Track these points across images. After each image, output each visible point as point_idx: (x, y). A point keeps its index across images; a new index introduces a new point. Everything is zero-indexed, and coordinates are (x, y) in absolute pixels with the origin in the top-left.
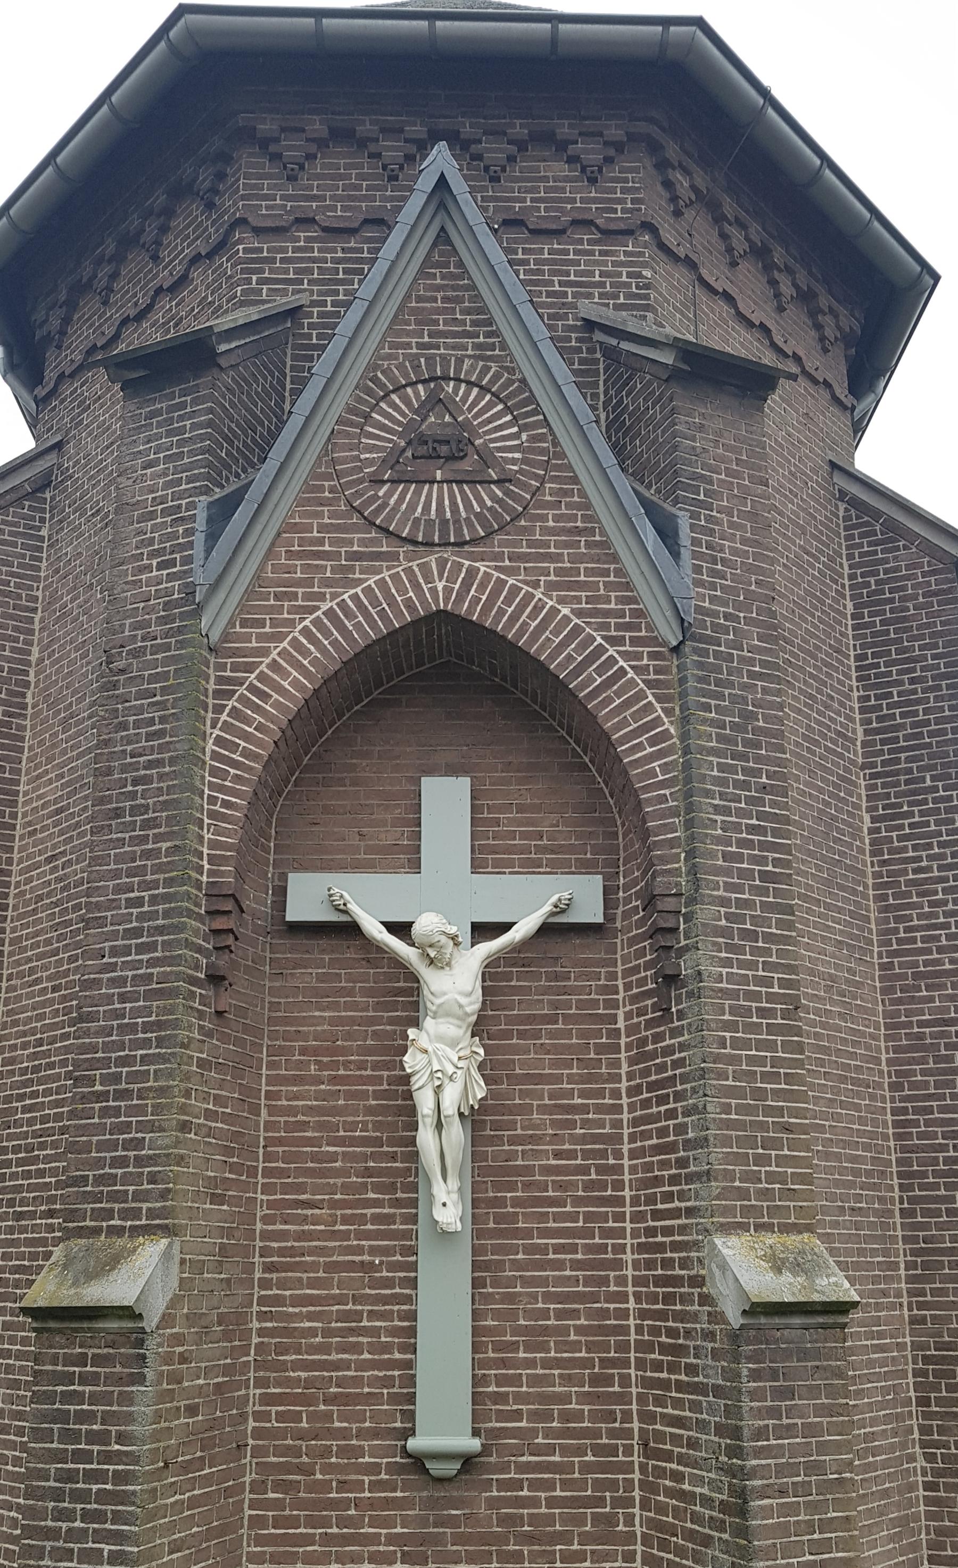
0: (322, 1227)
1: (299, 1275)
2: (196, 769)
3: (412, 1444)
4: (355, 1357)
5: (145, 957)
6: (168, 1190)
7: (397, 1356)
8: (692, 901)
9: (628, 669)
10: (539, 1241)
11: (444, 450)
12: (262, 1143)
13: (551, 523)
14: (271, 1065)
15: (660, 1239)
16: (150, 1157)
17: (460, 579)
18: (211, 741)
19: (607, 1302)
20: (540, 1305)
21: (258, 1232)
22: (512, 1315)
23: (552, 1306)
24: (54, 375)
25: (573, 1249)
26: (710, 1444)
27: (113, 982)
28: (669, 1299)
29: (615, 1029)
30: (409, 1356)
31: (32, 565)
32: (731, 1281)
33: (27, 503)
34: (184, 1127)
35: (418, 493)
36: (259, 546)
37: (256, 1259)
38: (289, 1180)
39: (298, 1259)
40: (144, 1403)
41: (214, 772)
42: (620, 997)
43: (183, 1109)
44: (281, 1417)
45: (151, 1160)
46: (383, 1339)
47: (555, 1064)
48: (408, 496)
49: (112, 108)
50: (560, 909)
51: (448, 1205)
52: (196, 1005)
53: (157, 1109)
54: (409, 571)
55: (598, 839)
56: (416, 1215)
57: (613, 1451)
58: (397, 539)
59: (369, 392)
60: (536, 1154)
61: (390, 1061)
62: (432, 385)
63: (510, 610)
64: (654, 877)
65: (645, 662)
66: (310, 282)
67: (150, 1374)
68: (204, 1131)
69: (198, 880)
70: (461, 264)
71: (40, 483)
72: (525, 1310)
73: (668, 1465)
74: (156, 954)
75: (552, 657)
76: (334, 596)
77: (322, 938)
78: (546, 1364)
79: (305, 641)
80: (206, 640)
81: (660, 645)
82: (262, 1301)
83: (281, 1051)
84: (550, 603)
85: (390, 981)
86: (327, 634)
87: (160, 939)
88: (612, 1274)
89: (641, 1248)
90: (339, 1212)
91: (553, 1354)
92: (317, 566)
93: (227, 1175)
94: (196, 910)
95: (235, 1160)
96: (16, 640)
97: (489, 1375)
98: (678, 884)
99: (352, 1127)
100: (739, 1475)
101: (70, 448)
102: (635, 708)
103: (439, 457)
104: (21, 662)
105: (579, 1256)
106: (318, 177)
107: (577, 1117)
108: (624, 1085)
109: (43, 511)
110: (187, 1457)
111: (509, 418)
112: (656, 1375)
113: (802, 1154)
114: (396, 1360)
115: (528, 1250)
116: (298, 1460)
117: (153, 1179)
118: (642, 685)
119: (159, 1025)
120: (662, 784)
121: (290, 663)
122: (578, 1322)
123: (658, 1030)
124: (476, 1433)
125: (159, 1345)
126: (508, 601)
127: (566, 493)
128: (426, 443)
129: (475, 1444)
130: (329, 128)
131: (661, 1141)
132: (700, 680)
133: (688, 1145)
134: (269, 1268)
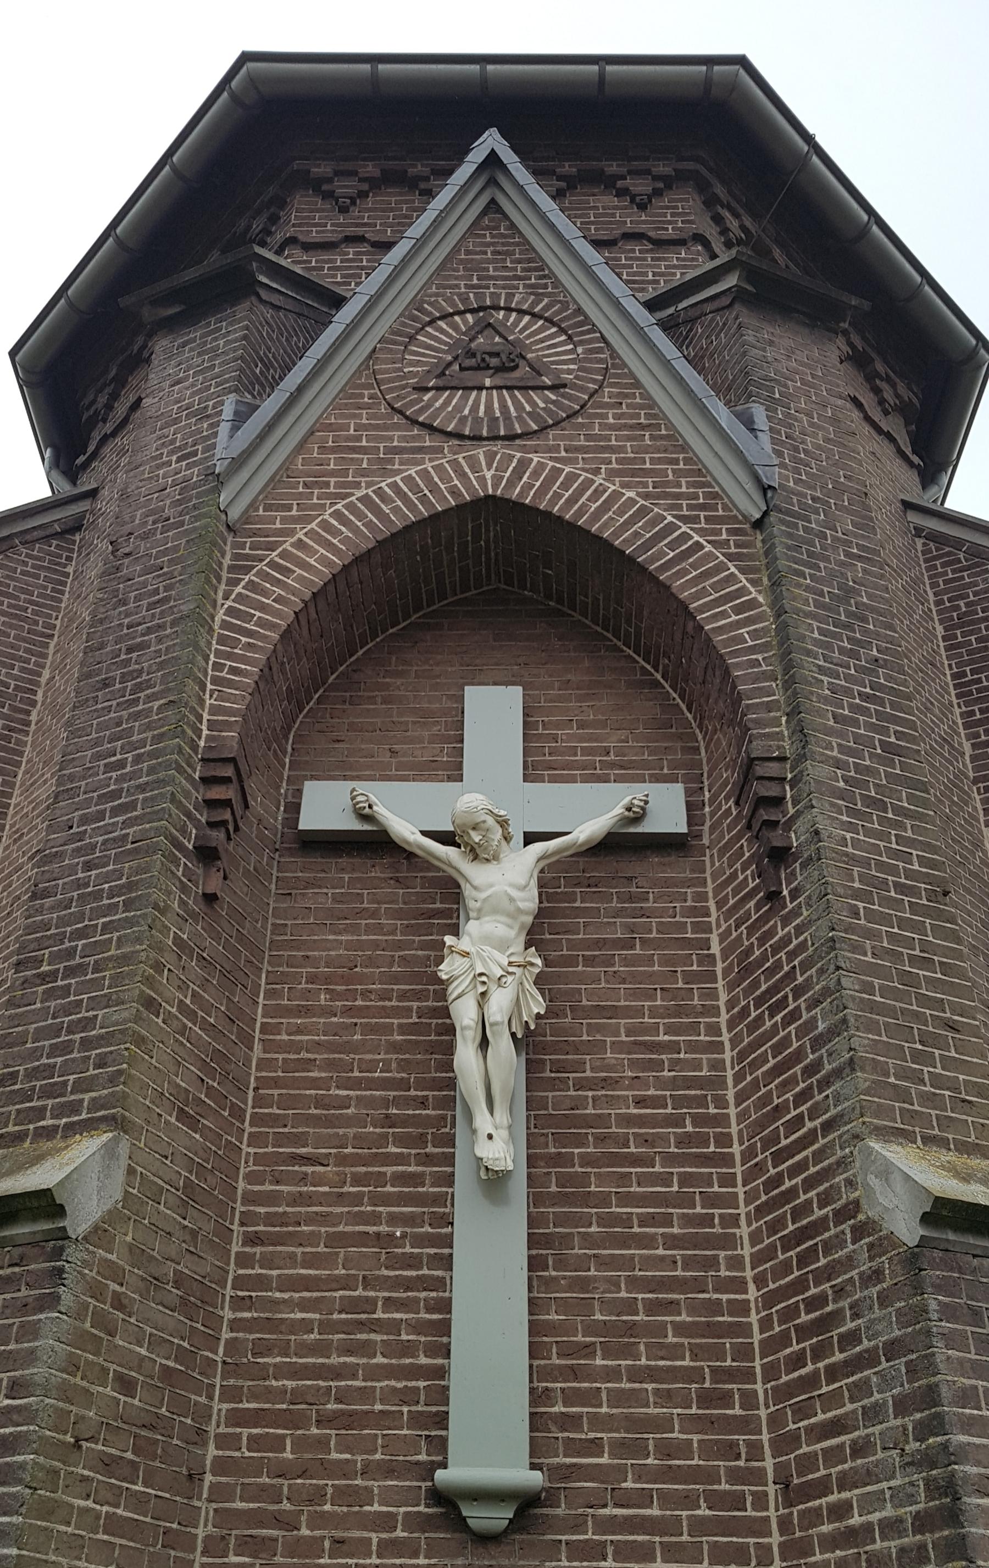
0: (326, 1189)
1: (292, 1249)
4: (364, 1360)
5: (120, 819)
6: (120, 1072)
7: (423, 1360)
8: (802, 757)
9: (705, 543)
10: (618, 1210)
11: (494, 362)
13: (611, 421)
14: (270, 994)
15: (788, 1184)
16: (101, 1037)
17: (511, 469)
18: (222, 612)
19: (716, 1290)
20: (623, 1294)
21: (240, 1192)
22: (585, 1306)
23: (640, 1296)
25: (667, 1221)
29: (709, 956)
30: (440, 1361)
32: (899, 1186)
33: (55, 542)
34: (150, 1004)
35: (465, 399)
38: (286, 1130)
39: (291, 1229)
40: (52, 1338)
41: (222, 640)
44: (254, 1443)
46: (404, 1337)
49: (173, 168)
50: (636, 815)
51: (494, 1139)
52: (180, 874)
54: (455, 464)
56: (453, 1174)
57: (738, 1502)
60: (611, 1101)
62: (481, 314)
63: (567, 495)
64: (750, 742)
65: (724, 536)
69: (193, 740)
70: (513, 226)
71: (71, 524)
75: (616, 534)
77: (341, 857)
78: (636, 1375)
79: (335, 523)
80: (223, 516)
81: (740, 523)
82: (239, 1282)
83: (283, 978)
85: (424, 902)
86: (361, 516)
87: (141, 797)
88: (722, 1254)
90: (347, 1170)
91: (643, 1361)
92: (352, 459)
93: (203, 1096)
94: (189, 770)
95: (215, 1085)
96: (27, 661)
97: (552, 1390)
101: (105, 492)
102: (715, 579)
103: (488, 367)
104: (31, 682)
105: (676, 1230)
106: (369, 210)
107: (664, 1057)
109: (72, 551)
110: (113, 1451)
113: (975, 1060)
114: (421, 1366)
115: (603, 1220)
116: (276, 1507)
118: (722, 558)
120: (752, 650)
121: (316, 544)
122: (678, 1319)
124: (533, 1467)
125: (85, 1263)
126: (565, 486)
127: (626, 396)
128: (474, 355)
129: (536, 1479)
131: (780, 1058)
132: (789, 548)
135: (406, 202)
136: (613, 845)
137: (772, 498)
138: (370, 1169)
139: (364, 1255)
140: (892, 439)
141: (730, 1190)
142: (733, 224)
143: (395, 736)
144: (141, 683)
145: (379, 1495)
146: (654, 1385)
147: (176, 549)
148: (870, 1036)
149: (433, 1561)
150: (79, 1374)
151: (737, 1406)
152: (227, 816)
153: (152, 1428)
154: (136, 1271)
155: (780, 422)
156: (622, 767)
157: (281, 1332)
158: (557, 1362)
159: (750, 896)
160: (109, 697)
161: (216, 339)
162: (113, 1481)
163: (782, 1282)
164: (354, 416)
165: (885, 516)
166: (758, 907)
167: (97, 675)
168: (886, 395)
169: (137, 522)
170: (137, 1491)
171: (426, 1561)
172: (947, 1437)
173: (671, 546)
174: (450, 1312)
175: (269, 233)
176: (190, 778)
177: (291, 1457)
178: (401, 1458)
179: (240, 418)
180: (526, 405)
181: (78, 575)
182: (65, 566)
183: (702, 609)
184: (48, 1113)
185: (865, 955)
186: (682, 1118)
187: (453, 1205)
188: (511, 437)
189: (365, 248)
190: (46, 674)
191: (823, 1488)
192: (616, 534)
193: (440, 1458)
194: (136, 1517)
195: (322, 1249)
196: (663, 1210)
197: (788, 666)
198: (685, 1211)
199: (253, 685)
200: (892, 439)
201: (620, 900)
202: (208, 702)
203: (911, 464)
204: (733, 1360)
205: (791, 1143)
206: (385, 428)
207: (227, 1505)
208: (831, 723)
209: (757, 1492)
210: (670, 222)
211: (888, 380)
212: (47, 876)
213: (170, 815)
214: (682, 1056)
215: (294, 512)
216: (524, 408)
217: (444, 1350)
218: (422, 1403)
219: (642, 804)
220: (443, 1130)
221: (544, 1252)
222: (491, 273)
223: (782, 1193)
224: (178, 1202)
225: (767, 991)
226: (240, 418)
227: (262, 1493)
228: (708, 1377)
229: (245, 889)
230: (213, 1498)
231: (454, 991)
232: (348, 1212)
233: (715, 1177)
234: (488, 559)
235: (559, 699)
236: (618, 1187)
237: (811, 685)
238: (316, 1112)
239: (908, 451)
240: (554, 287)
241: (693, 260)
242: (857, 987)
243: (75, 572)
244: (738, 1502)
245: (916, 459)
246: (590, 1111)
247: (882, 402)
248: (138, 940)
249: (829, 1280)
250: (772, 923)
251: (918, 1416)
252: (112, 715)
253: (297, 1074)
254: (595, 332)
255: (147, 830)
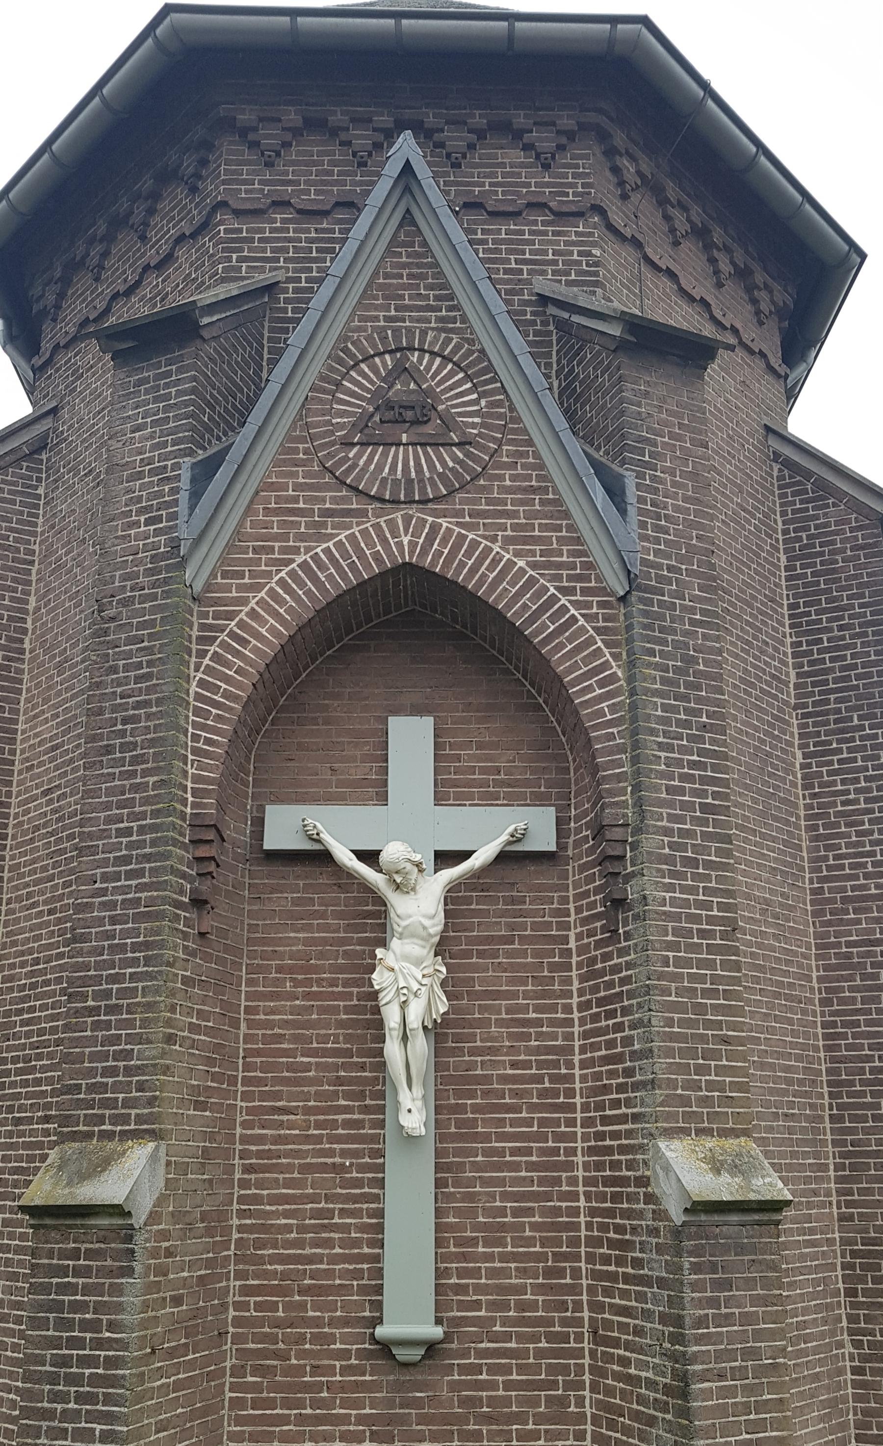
0: (297, 1132)
1: (276, 1175)
2: (180, 709)
3: (380, 1331)
4: (327, 1251)
5: (134, 883)
6: (155, 1098)
7: (366, 1250)
8: (638, 831)
9: (579, 617)
10: (497, 1145)
11: (409, 415)
12: (242, 1055)
13: (508, 483)
14: (249, 983)
15: (608, 1142)
16: (138, 1067)
17: (424, 534)
18: (195, 684)
19: (559, 1200)
20: (498, 1204)
21: (238, 1136)
22: (472, 1213)
23: (509, 1205)
24: (50, 346)
25: (528, 1152)
26: (655, 1332)
27: (104, 906)
28: (616, 1198)
29: (567, 949)
30: (377, 1251)
31: (29, 521)
32: (674, 1182)
33: (25, 464)
34: (170, 1039)
35: (385, 455)
36: (239, 503)
37: (236, 1161)
38: (267, 1088)
39: (274, 1161)
40: (133, 1293)
41: (197, 712)
42: (572, 919)
43: (169, 1023)
44: (259, 1306)
45: (140, 1070)
46: (353, 1235)
47: (511, 981)
48: (377, 458)
49: (103, 99)
50: (516, 838)
51: (413, 1112)
52: (181, 927)
53: (145, 1023)
54: (377, 527)
55: (551, 774)
56: (384, 1120)
57: (565, 1338)
58: (366, 497)
59: (341, 362)
60: (494, 1064)
61: (360, 979)
62: (398, 355)
63: (470, 563)
64: (602, 809)
65: (595, 610)
66: (286, 260)
67: (138, 1267)
68: (188, 1043)
69: (182, 811)
70: (425, 244)
71: (37, 445)
72: (484, 1208)
73: (616, 1351)
74: (144, 880)
75: (509, 606)
76: (308, 550)
77: (297, 865)
78: (503, 1258)
79: (281, 592)
80: (190, 590)
82: (242, 1200)
83: (259, 969)
84: (507, 556)
85: (359, 905)
86: (301, 584)
87: (147, 866)
88: (564, 1175)
89: (591, 1151)
90: (312, 1118)
91: (509, 1249)
92: (292, 522)
93: (209, 1084)
94: (181, 839)
95: (217, 1069)
96: (15, 590)
97: (451, 1268)
98: (625, 815)
99: (325, 1039)
100: (681, 1360)
102: (585, 653)
103: (405, 421)
104: (19, 610)
105: (534, 1159)
106: (293, 163)
107: (532, 1030)
108: (575, 1000)
109: (40, 471)
110: (173, 1344)
111: (469, 385)
112: (605, 1268)
113: (739, 1064)
114: (365, 1254)
115: (486, 1152)
116: (275, 1347)
117: (141, 1087)
118: (592, 632)
119: (147, 946)
120: (610, 723)
121: (267, 612)
122: (533, 1220)
123: (606, 950)
124: (438, 1321)
125: (147, 1240)
126: (468, 554)
128: (393, 408)
129: (438, 1332)
130: (303, 118)
131: (609, 1052)
132: (646, 627)
133: (634, 1056)
134: (248, 1169)
136: (503, 857)
176: (184, 846)
190: (32, 600)
229: (227, 907)
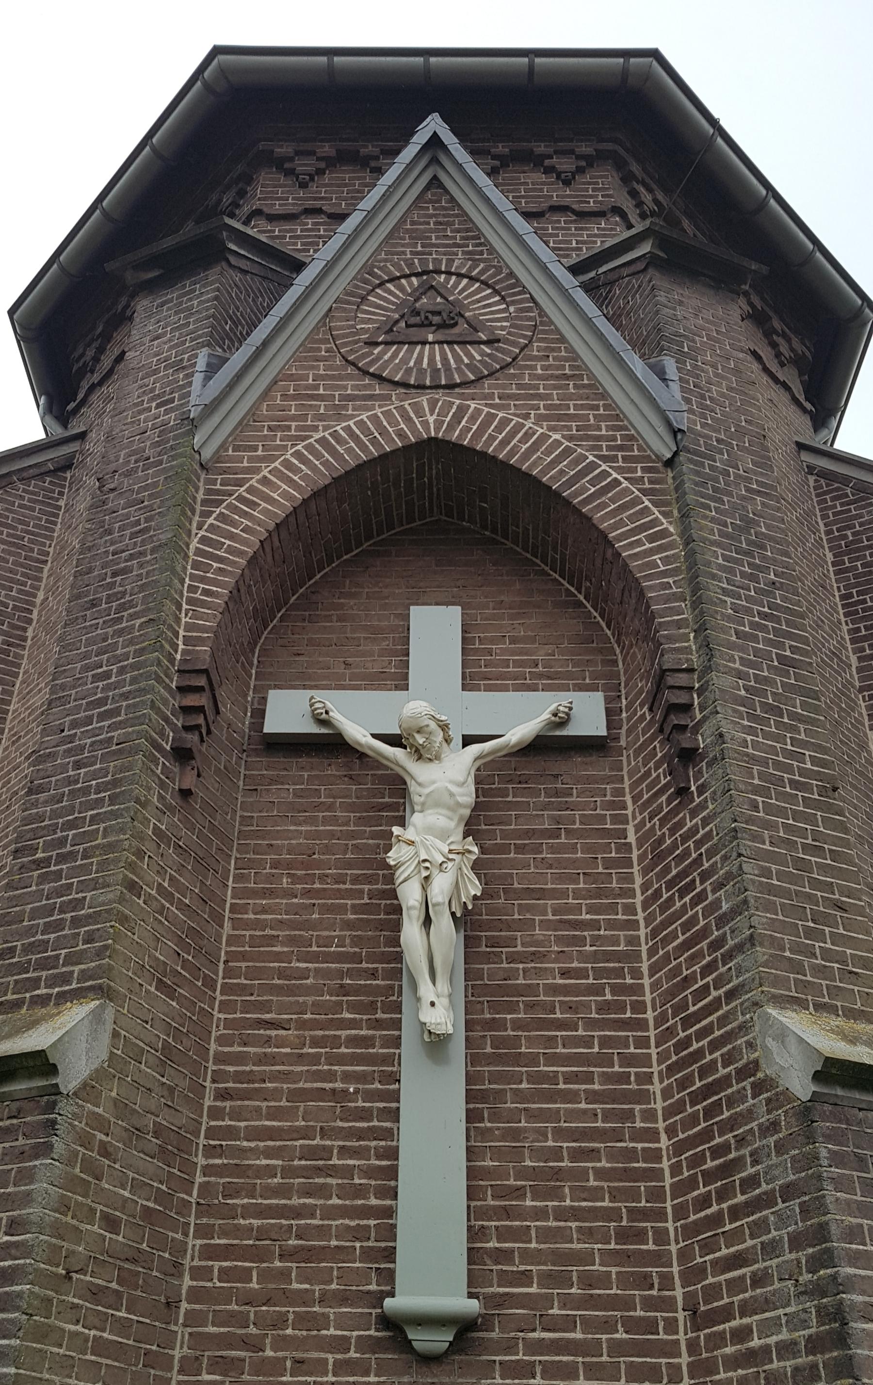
0: (288, 1050)
1: (258, 1103)
4: (322, 1202)
5: (106, 723)
6: (106, 947)
7: (374, 1201)
8: (708, 669)
9: (622, 480)
10: (546, 1069)
11: (436, 319)
13: (540, 371)
14: (238, 878)
15: (695, 1046)
16: (89, 916)
17: (451, 414)
18: (196, 540)
19: (632, 1140)
20: (550, 1143)
21: (212, 1053)
22: (517, 1154)
23: (565, 1145)
25: (588, 1078)
29: (625, 844)
30: (388, 1202)
32: (793, 1048)
33: (48, 479)
34: (133, 887)
35: (410, 352)
38: (253, 998)
39: (256, 1085)
40: (46, 1181)
41: (196, 565)
44: (224, 1274)
46: (357, 1181)
49: (153, 149)
50: (561, 720)
51: (436, 1006)
52: (159, 772)
54: (401, 409)
56: (400, 1037)
57: (651, 1326)
60: (540, 973)
62: (425, 277)
63: (500, 437)
64: (662, 655)
65: (639, 474)
69: (170, 654)
70: (452, 199)
71: (62, 463)
75: (544, 472)
77: (301, 757)
78: (561, 1214)
79: (296, 462)
80: (197, 456)
81: (654, 462)
82: (211, 1133)
83: (250, 864)
85: (374, 797)
86: (318, 456)
87: (124, 704)
88: (638, 1107)
90: (307, 1033)
91: (568, 1202)
92: (311, 405)
93: (179, 968)
94: (167, 681)
95: (190, 958)
96: (24, 584)
97: (488, 1227)
101: (93, 435)
102: (631, 512)
103: (431, 324)
104: (27, 602)
105: (596, 1087)
106: (326, 185)
107: (586, 933)
109: (64, 486)
110: (100, 1282)
113: (861, 936)
114: (372, 1207)
115: (532, 1078)
116: (243, 1331)
118: (637, 493)
120: (664, 574)
121: (279, 481)
122: (598, 1165)
124: (471, 1295)
125: (75, 1116)
126: (499, 429)
127: (553, 350)
128: (418, 314)
129: (473, 1306)
131: (688, 934)
132: (696, 484)
135: (359, 178)
137: (682, 440)
138: (327, 1033)
139: (321, 1108)
140: (787, 388)
141: (644, 1051)
142: (647, 198)
143: (348, 650)
144: (124, 603)
145: (335, 1320)
146: (577, 1224)
147: (155, 485)
148: (768, 915)
149: (382, 1379)
150: (70, 1214)
151: (651, 1242)
152: (201, 720)
153: (134, 1261)
154: (120, 1122)
155: (689, 373)
156: (549, 678)
157: (248, 1177)
158: (492, 1203)
159: (662, 791)
160: (96, 616)
161: (190, 300)
162: (100, 1308)
163: (690, 1133)
164: (313, 368)
165: (781, 455)
166: (669, 801)
167: (86, 596)
168: (782, 349)
169: (121, 461)
170: (121, 1317)
171: (376, 1379)
172: (836, 1269)
173: (592, 483)
174: (397, 1159)
175: (238, 206)
176: (167, 688)
177: (257, 1287)
178: (354, 1288)
179: (212, 370)
180: (464, 358)
181: (68, 508)
182: (57, 500)
183: (619, 538)
184: (43, 983)
185: (764, 843)
186: (602, 987)
187: (400, 1065)
188: (451, 386)
189: (322, 219)
190: (41, 595)
191: (726, 1314)
192: (544, 472)
193: (389, 1288)
194: (120, 1340)
195: (284, 1103)
196: (585, 1069)
197: (696, 588)
198: (605, 1069)
199: (223, 605)
200: (787, 388)
201: (548, 795)
202: (184, 620)
203: (804, 410)
204: (647, 1201)
205: (699, 1009)
206: (340, 378)
207: (200, 1329)
208: (734, 638)
209: (668, 1318)
210: (591, 197)
211: (784, 335)
212: (42, 774)
213: (150, 720)
214: (602, 933)
215: (259, 453)
216: (463, 361)
217: (392, 1192)
218: (372, 1239)
219: (567, 710)
220: (391, 998)
221: (480, 1106)
222: (434, 241)
223: (691, 1054)
224: (157, 1062)
225: (677, 875)
226: (212, 370)
227: (231, 1319)
228: (625, 1216)
229: (217, 785)
230: (188, 1323)
231: (401, 875)
232: (307, 1071)
233: (631, 1039)
234: (431, 494)
235: (494, 617)
236: (546, 1048)
237: (716, 605)
238: (279, 982)
239: (802, 398)
240: (489, 254)
241: (611, 229)
242: (756, 872)
243: (66, 505)
244: (651, 1326)
245: (808, 406)
246: (521, 981)
247: (778, 355)
248: (122, 830)
249: (732, 1131)
250: (681, 815)
251: (810, 1250)
252: (99, 631)
253: (262, 949)
254: (525, 293)
255: (129, 733)
